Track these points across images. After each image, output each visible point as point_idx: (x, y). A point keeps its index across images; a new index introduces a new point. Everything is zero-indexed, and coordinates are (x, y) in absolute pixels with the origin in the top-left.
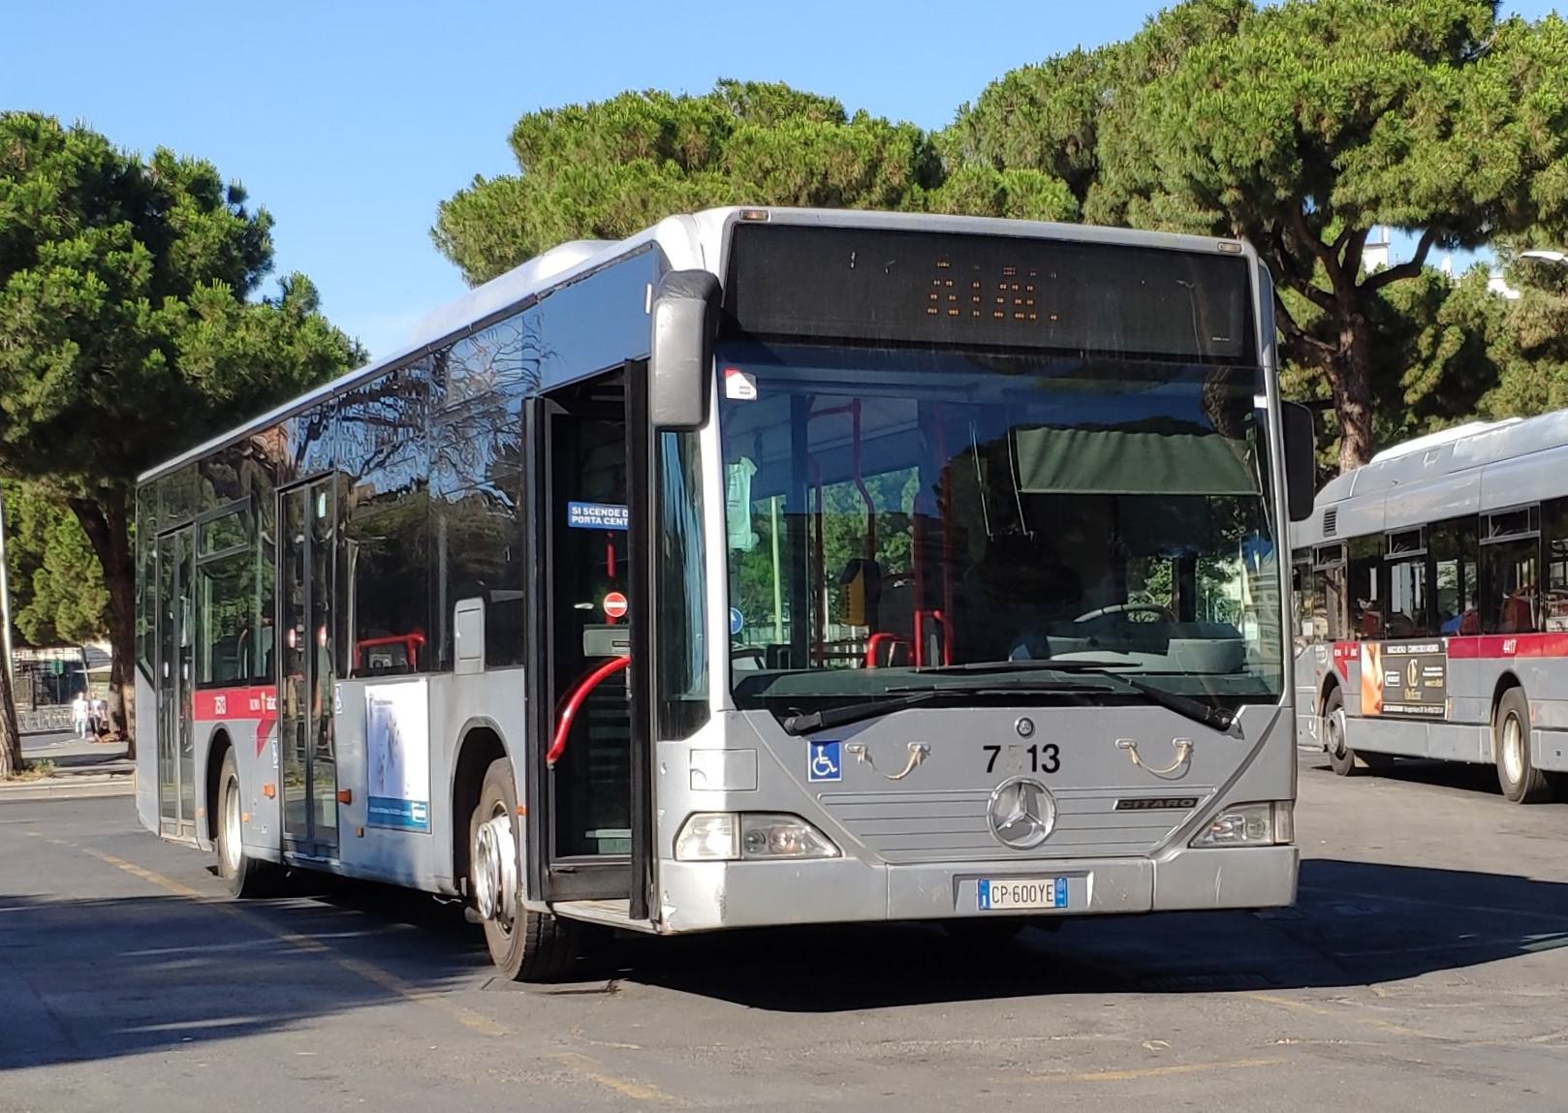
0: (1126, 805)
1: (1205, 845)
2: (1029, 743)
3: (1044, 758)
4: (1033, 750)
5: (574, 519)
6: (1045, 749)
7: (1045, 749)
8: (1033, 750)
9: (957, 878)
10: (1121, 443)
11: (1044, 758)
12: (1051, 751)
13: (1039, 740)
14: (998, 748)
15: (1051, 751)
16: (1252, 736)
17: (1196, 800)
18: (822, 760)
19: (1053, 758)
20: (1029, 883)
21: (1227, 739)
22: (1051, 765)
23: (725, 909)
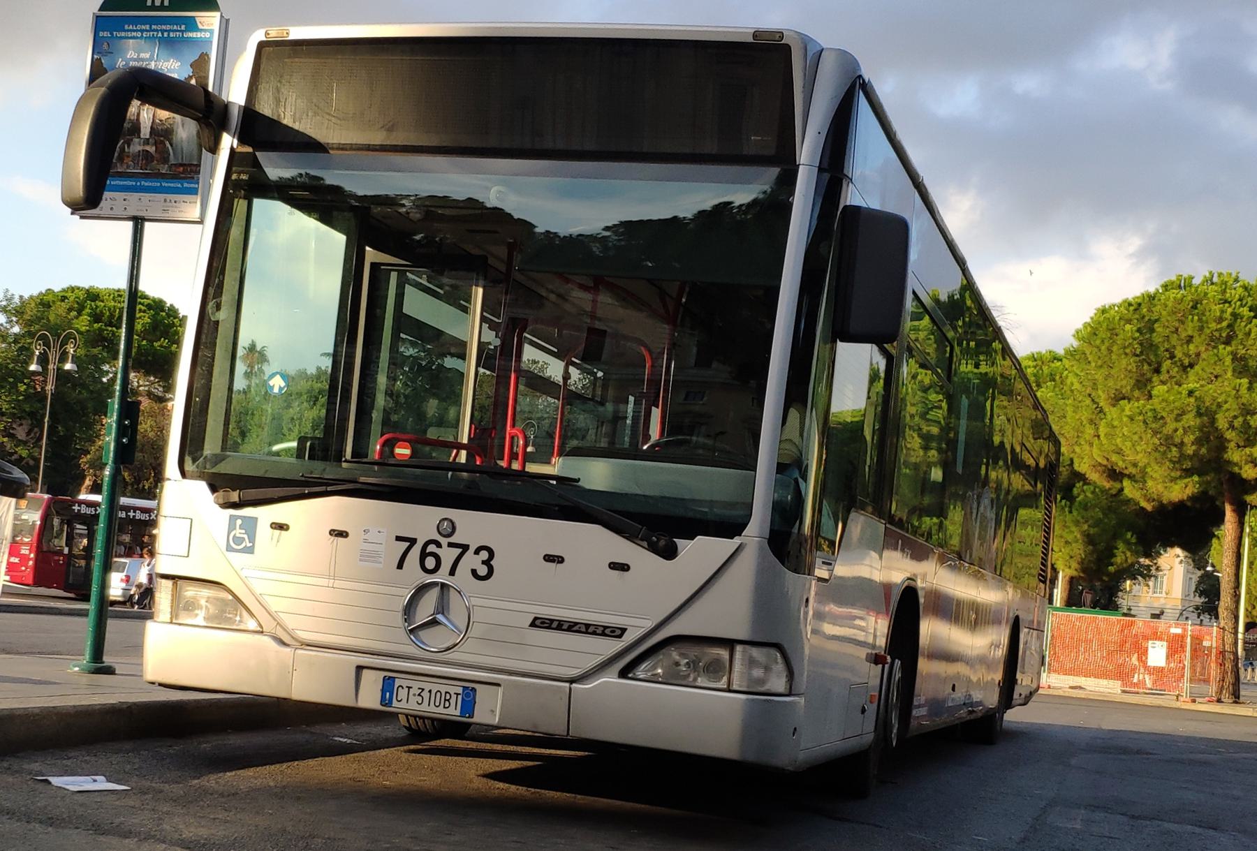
0: (540, 623)
6: (477, 552)
7: (477, 552)
12: (484, 555)
14: (413, 541)
15: (484, 555)
17: (624, 630)
18: (238, 532)
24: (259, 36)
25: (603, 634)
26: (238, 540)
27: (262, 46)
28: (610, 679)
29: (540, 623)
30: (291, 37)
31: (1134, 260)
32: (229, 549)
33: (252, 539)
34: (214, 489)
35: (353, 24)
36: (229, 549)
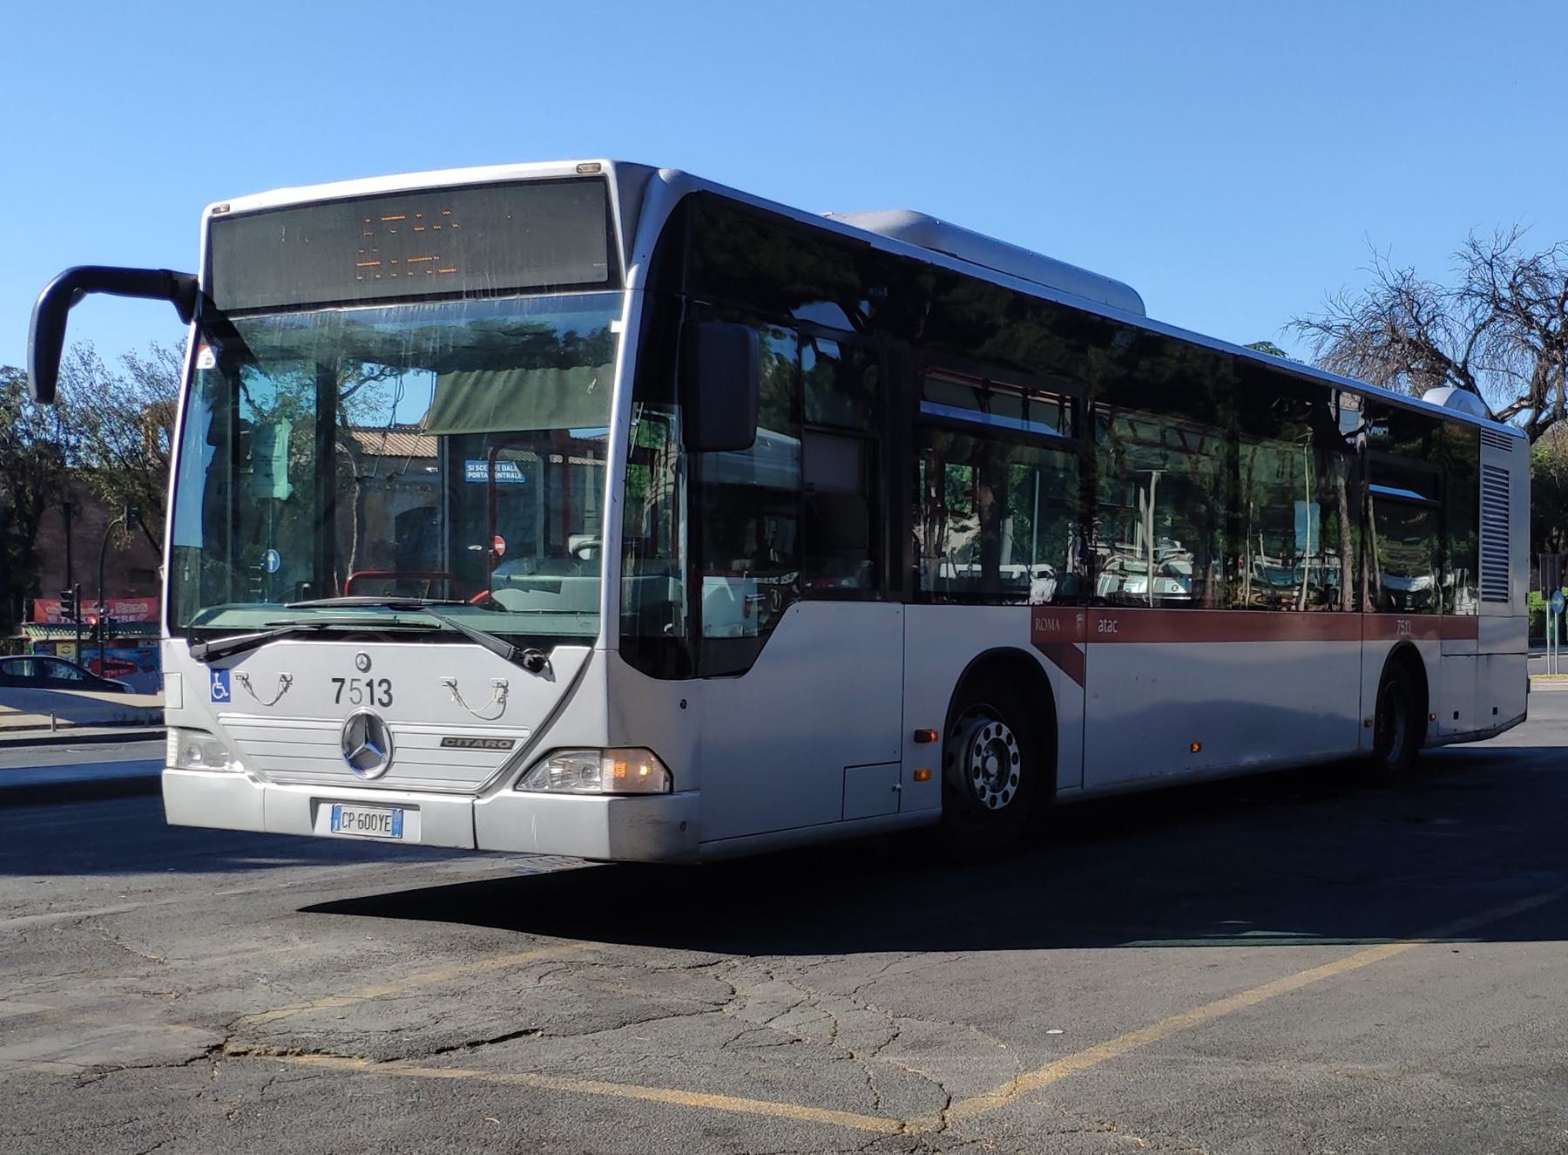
0: (449, 742)
1: (537, 787)
2: (366, 677)
3: (379, 692)
4: (370, 684)
5: (470, 475)
6: (380, 684)
7: (380, 684)
8: (370, 684)
9: (315, 802)
10: (521, 380)
11: (379, 692)
12: (385, 686)
13: (375, 674)
14: (342, 681)
15: (385, 686)
16: (564, 675)
17: (513, 742)
18: (218, 685)
19: (386, 692)
20: (372, 811)
21: (539, 681)
22: (385, 699)
23: (612, 848)
24: (207, 213)
25: (463, 745)
26: (218, 691)
27: (211, 221)
28: (507, 792)
29: (449, 742)
30: (232, 210)
31: (598, 332)
32: (214, 700)
33: (228, 690)
34: (191, 643)
35: (247, 194)
36: (214, 700)
